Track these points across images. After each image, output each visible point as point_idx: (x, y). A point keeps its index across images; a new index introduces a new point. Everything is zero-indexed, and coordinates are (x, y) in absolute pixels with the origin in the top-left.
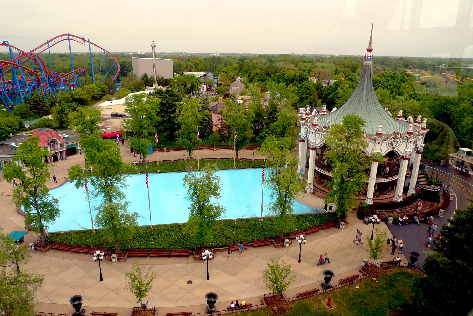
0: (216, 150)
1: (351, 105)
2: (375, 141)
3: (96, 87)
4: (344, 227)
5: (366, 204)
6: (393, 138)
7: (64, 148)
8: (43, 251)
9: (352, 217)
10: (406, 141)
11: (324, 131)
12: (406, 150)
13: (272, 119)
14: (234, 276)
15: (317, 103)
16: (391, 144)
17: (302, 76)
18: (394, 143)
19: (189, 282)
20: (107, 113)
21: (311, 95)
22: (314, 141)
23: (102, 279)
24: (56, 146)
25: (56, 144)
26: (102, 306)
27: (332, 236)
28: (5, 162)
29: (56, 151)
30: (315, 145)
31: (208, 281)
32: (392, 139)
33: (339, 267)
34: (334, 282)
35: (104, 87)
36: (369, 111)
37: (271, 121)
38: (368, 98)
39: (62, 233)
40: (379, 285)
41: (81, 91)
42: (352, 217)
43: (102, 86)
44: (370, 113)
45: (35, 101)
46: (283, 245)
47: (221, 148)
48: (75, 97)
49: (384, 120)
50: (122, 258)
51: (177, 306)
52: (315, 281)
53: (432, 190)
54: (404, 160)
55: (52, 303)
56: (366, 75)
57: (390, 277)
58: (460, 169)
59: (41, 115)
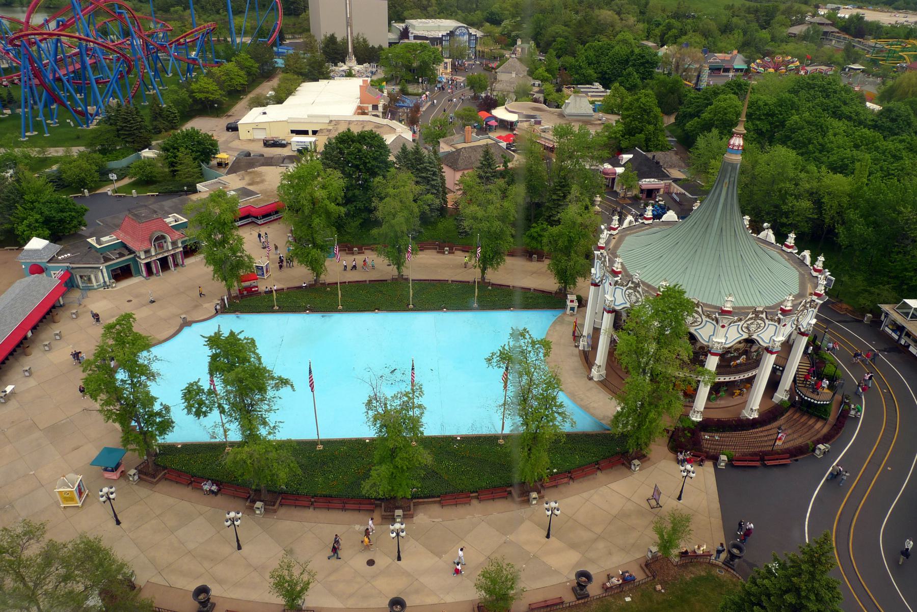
0: (449, 253)
1: (691, 235)
2: (717, 323)
3: (236, 69)
4: (637, 469)
5: (690, 419)
6: (751, 319)
7: (178, 247)
8: (152, 483)
9: (659, 448)
10: (776, 324)
11: (630, 288)
12: (773, 338)
13: (556, 202)
14: (440, 557)
15: (659, 141)
16: (748, 328)
17: (644, 56)
18: (753, 327)
19: (371, 563)
20: (256, 137)
21: (649, 123)
22: (613, 299)
23: (239, 548)
24: (165, 245)
25: (165, 242)
26: (239, 597)
27: (615, 486)
28: (81, 277)
29: (166, 254)
30: (613, 306)
31: (399, 562)
32: (748, 320)
33: (610, 554)
34: (593, 589)
35: (252, 66)
36: (722, 253)
37: (555, 204)
38: (724, 224)
39: (179, 446)
40: (665, 598)
41: (209, 84)
42: (659, 448)
43: (248, 64)
44: (722, 256)
45: (126, 120)
46: (528, 500)
47: (459, 250)
48: (199, 96)
49: (746, 271)
50: (271, 507)
51: (348, 606)
52: (565, 580)
53: (816, 402)
54: (769, 354)
55: (167, 585)
56: (727, 180)
57: (686, 584)
58: (897, 337)
59: (136, 147)
